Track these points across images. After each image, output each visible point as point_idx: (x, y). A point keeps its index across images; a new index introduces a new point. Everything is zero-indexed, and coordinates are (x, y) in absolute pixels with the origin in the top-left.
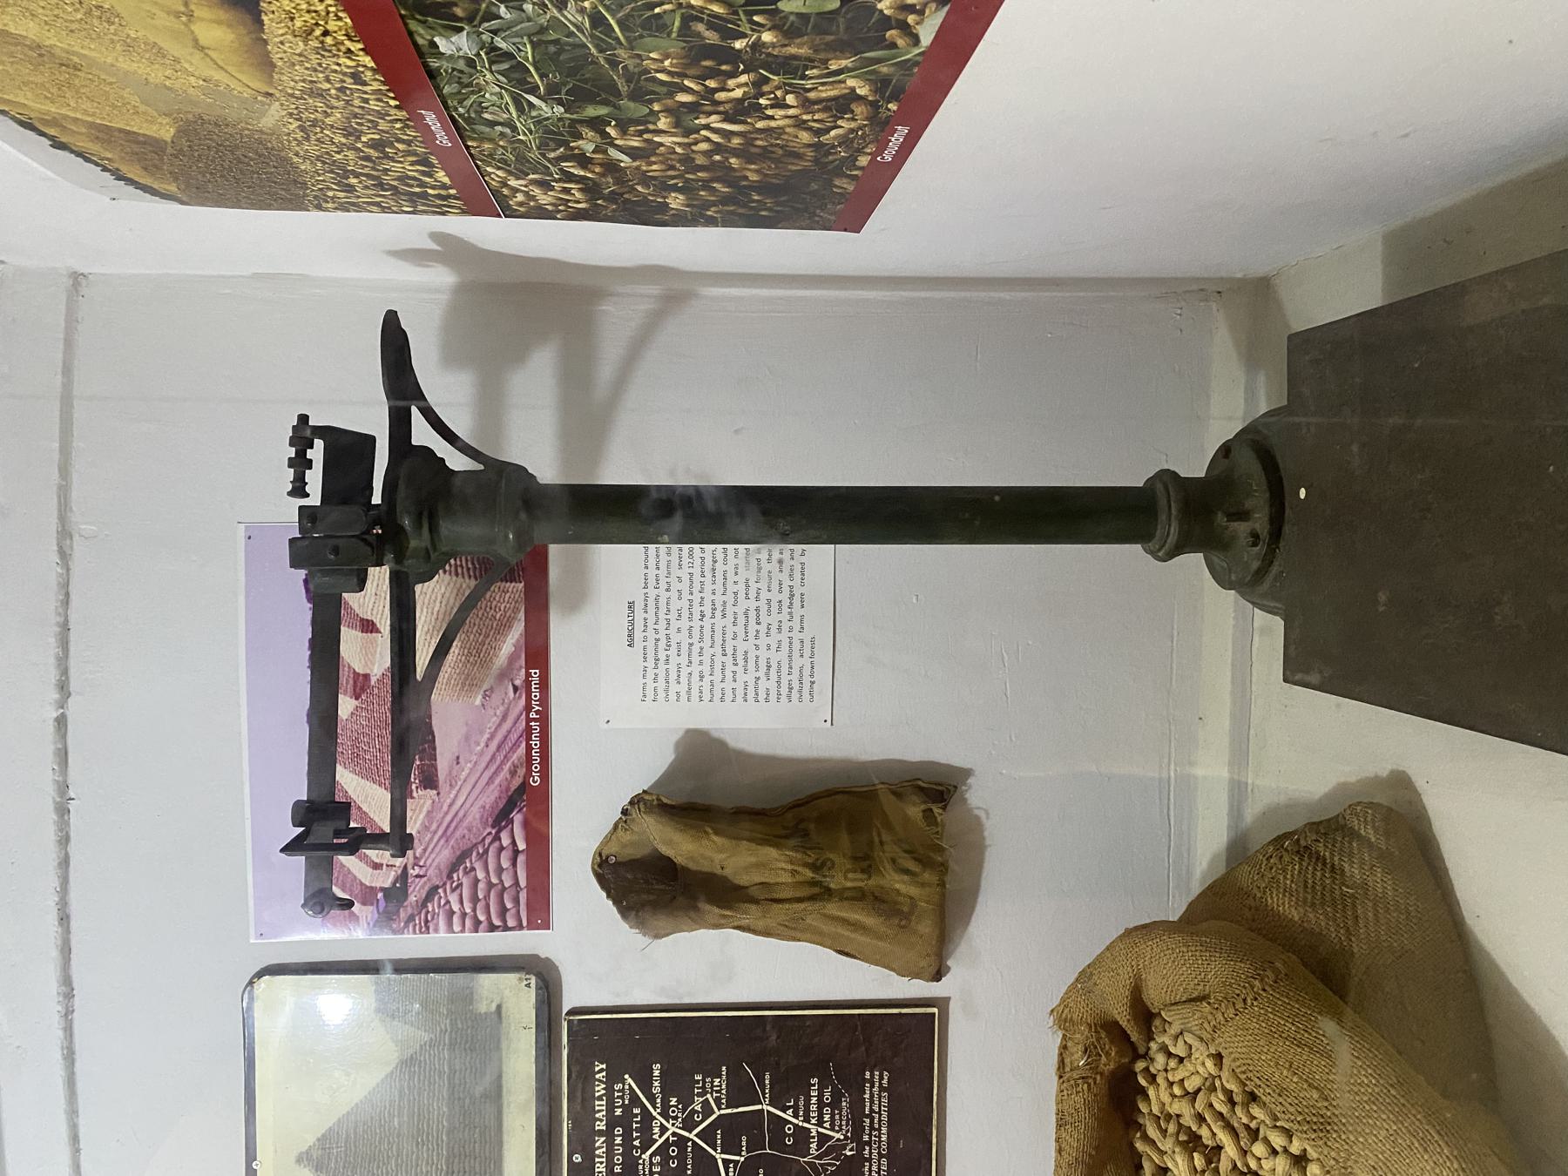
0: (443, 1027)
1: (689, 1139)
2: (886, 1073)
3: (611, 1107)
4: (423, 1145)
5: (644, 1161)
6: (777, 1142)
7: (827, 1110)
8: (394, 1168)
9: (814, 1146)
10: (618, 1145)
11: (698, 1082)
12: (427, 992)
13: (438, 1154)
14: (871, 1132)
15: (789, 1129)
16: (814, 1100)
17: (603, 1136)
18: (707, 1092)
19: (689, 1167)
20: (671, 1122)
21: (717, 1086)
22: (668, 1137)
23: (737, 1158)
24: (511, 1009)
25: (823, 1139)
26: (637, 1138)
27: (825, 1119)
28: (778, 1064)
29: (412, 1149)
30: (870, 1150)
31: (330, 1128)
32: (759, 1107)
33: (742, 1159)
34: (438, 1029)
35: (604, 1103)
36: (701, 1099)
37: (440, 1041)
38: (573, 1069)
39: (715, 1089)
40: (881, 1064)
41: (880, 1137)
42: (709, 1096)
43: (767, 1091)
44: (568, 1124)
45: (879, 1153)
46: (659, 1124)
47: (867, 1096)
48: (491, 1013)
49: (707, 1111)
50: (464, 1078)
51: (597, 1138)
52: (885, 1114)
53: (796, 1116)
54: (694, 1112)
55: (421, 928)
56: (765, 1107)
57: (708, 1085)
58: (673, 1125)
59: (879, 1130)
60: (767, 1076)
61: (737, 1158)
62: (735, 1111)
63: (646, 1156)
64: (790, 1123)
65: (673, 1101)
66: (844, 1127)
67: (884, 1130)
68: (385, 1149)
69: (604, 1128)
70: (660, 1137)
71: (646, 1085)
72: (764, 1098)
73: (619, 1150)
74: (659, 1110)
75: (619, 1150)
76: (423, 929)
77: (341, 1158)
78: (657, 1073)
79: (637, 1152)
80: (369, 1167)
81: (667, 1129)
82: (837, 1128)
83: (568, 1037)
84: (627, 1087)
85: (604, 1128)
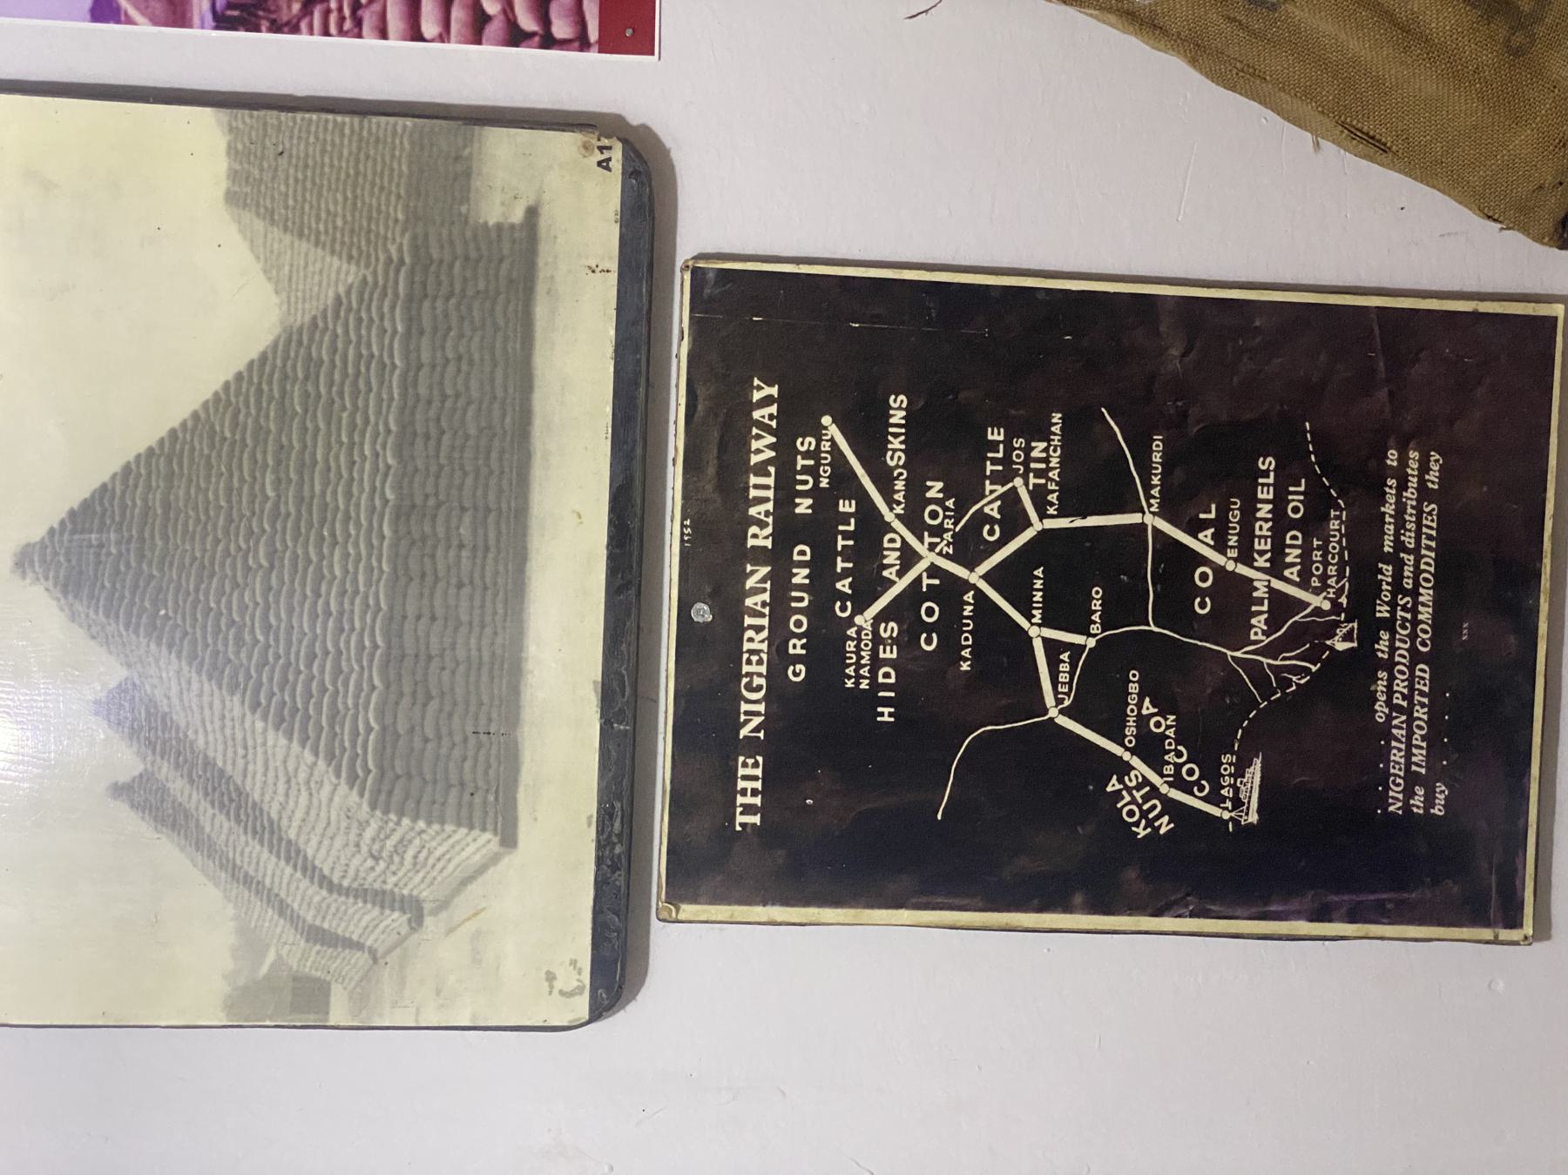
0: (393, 250)
1: (967, 586)
2: (1435, 456)
3: (786, 493)
4: (335, 543)
5: (859, 632)
6: (1175, 608)
7: (1294, 538)
8: (259, 599)
9: (1259, 622)
10: (800, 587)
11: (994, 446)
12: (357, 161)
13: (369, 569)
14: (1394, 596)
15: (1204, 577)
16: (1264, 510)
17: (764, 564)
18: (1016, 473)
19: (966, 653)
20: (927, 540)
21: (1038, 460)
22: (920, 577)
23: (1078, 639)
24: (555, 218)
25: (1282, 606)
26: (846, 573)
27: (1289, 559)
28: (1184, 415)
29: (307, 553)
30: (1392, 640)
31: (104, 487)
32: (1135, 518)
33: (1091, 643)
34: (382, 257)
35: (770, 481)
36: (1000, 490)
37: (385, 287)
38: (701, 392)
39: (1033, 465)
40: (1420, 436)
41: (1414, 611)
42: (1018, 482)
43: (1156, 481)
44: (683, 526)
45: (1413, 651)
46: (898, 545)
47: (1389, 509)
48: (512, 226)
49: (1013, 520)
50: (441, 383)
51: (749, 568)
52: (1429, 556)
53: (1220, 545)
54: (982, 518)
55: (342, 19)
56: (1149, 519)
57: (1018, 456)
58: (932, 547)
59: (1415, 593)
60: (1158, 445)
61: (1078, 639)
62: (1079, 523)
63: (864, 620)
64: (1205, 561)
65: (935, 489)
66: (1332, 581)
67: (1426, 595)
68: (239, 548)
69: (768, 543)
70: (900, 574)
71: (870, 441)
72: (1149, 497)
73: (801, 599)
74: (899, 510)
75: (801, 599)
76: (348, 25)
77: (128, 566)
78: (898, 417)
79: (843, 609)
80: (197, 590)
81: (920, 558)
82: (1315, 583)
83: (692, 311)
84: (826, 446)
85: (768, 543)
